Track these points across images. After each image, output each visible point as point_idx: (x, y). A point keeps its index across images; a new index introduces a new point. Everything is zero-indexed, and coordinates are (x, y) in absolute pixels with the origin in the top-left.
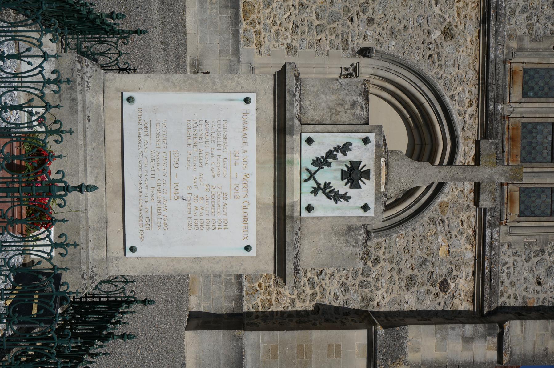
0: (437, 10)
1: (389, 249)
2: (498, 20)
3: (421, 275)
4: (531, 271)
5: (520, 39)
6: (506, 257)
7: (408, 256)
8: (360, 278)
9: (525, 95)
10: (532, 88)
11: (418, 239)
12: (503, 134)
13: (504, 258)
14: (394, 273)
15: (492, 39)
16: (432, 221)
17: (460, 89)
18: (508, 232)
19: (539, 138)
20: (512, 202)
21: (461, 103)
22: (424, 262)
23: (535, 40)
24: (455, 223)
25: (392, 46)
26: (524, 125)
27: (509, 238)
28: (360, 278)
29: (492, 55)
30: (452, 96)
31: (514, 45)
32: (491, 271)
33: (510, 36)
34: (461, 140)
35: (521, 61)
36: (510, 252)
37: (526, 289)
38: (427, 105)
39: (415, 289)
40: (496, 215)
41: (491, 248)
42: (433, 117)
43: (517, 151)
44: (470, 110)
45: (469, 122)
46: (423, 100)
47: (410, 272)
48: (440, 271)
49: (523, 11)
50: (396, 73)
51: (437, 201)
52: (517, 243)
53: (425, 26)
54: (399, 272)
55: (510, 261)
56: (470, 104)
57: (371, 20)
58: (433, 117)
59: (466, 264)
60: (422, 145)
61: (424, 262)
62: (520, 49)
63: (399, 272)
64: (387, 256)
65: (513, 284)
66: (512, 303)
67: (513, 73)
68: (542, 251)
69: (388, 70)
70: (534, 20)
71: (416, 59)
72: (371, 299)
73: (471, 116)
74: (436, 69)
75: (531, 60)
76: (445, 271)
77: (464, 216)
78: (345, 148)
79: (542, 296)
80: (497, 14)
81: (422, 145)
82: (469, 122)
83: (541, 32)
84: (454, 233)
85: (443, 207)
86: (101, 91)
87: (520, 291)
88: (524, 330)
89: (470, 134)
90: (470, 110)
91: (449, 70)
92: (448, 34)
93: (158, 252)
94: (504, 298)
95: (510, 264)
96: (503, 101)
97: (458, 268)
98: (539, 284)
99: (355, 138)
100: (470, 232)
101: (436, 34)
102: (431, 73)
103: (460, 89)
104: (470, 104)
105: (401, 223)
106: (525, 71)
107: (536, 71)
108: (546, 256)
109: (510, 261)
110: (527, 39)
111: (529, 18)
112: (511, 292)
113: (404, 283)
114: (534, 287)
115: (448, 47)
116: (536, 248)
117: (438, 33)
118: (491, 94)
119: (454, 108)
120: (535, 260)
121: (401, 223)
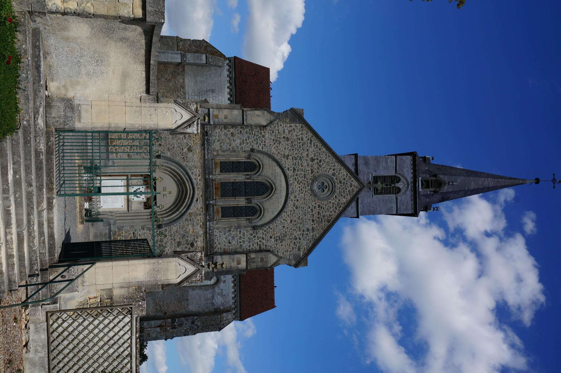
0: (185, 141)
1: (170, 231)
2: (208, 144)
3: (183, 241)
4: (226, 238)
5: (217, 151)
6: (216, 233)
7: (178, 234)
8: (159, 243)
9: (221, 171)
10: (224, 169)
11: (181, 227)
12: (213, 186)
13: (215, 233)
14: (173, 241)
15: (206, 152)
16: (187, 220)
17: (195, 170)
18: (216, 224)
19: (228, 188)
20: (218, 212)
21: (196, 175)
22: (184, 236)
23: (223, 151)
24: (195, 221)
25: (168, 154)
26: (222, 183)
27: (217, 226)
28: (159, 243)
29: (206, 158)
30: (192, 173)
31: (215, 153)
32: (210, 238)
33: (214, 150)
34: (196, 189)
35: (219, 159)
36: (217, 231)
37: (225, 245)
38: (183, 176)
39: (181, 247)
40: (211, 217)
41: (210, 230)
42: (186, 180)
43: (219, 193)
44: (199, 178)
45: (199, 182)
46: (181, 174)
47: (179, 240)
48: (190, 239)
49: (218, 141)
50: (170, 164)
51: (188, 212)
52: (220, 227)
53: (181, 147)
54: (175, 240)
55: (218, 235)
56: (199, 176)
57: (160, 145)
58: (186, 180)
59: (200, 236)
60: (183, 191)
61: (184, 236)
62: (218, 155)
63: (175, 240)
64: (169, 234)
65: (219, 244)
66: (220, 251)
67: (216, 163)
68: (230, 230)
69: (168, 163)
70: (222, 144)
71: (178, 159)
72: (164, 251)
73: (200, 180)
74: (186, 163)
75: (223, 159)
76: (192, 239)
77: (198, 218)
78: (139, 189)
79: (231, 248)
80: (208, 142)
81: (183, 191)
82: (199, 182)
83: (225, 148)
84: (195, 224)
85: (190, 214)
86: (461, 244)
87: (223, 247)
88: (222, 259)
89: (199, 187)
90: (199, 178)
91: (191, 163)
92: (190, 150)
93: (107, 207)
94: (216, 249)
95: (218, 236)
96: (212, 174)
97: (197, 238)
98: (230, 243)
99: (141, 187)
100: (201, 224)
101: (185, 150)
102: (184, 164)
103: (195, 170)
104: (199, 176)
105: (174, 221)
106: (221, 162)
107: (225, 162)
108: (231, 232)
109: (218, 235)
110: (220, 151)
111: (221, 143)
112: (219, 246)
113: (176, 244)
114: (227, 244)
115: (190, 155)
116: (227, 229)
117: (186, 149)
118: (207, 172)
119: (193, 177)
120: (227, 234)
121: (174, 221)
